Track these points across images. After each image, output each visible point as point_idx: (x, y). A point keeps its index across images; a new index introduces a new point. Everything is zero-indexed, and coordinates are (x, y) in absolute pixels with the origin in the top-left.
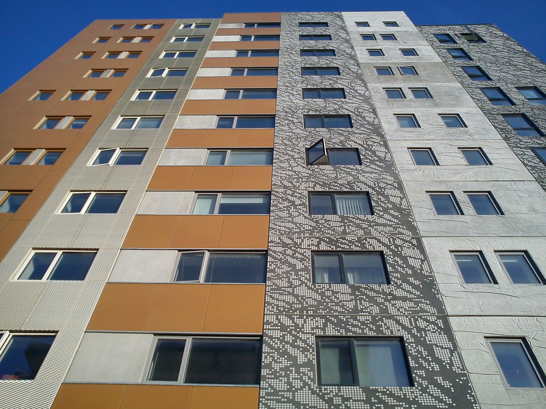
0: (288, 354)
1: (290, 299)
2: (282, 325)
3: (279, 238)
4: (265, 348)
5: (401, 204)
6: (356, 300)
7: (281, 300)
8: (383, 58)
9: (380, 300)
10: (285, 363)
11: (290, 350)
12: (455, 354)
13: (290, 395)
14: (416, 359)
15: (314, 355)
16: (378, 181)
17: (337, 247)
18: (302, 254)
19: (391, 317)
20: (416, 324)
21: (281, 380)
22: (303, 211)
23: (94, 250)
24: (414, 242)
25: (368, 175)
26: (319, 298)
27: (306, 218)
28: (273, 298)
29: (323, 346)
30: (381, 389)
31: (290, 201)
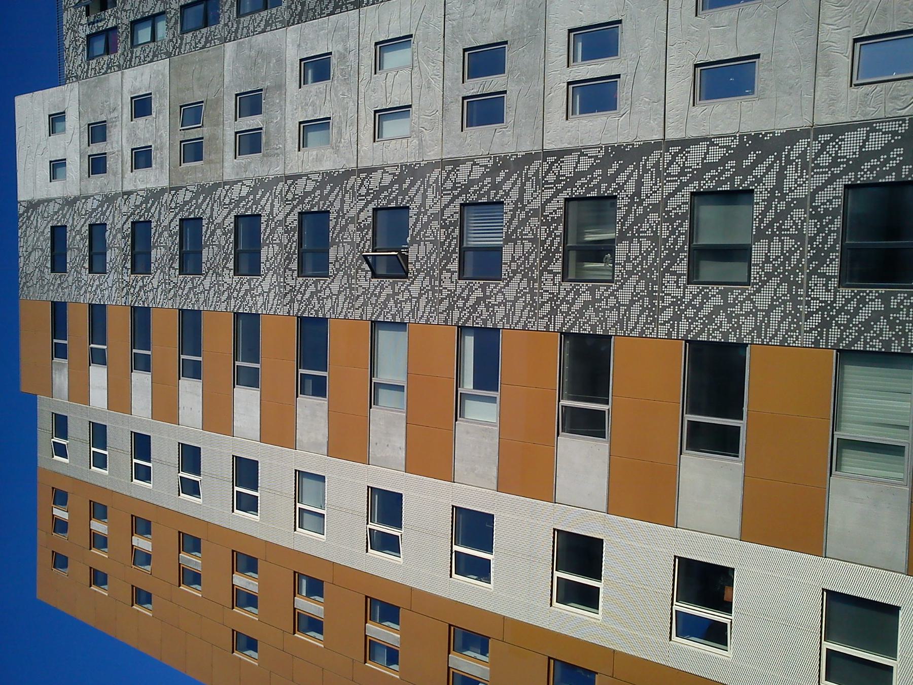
0: (711, 314)
1: (272, 295)
2: (672, 319)
3: (542, 318)
4: (575, 330)
5: (317, 181)
6: (522, 239)
7: (638, 319)
8: (157, 149)
9: (425, 219)
10: (315, 301)
11: (576, 307)
12: (387, 169)
13: (509, 305)
14: (589, 190)
15: (871, 292)
16: (285, 201)
17: (454, 251)
18: (301, 285)
19: (543, 206)
20: (551, 183)
21: (743, 323)
22: (495, 288)
23: (675, 561)
24: (363, 175)
25: (116, 219)
26: (519, 276)
27: (507, 285)
28: (422, 316)
29: (697, 277)
30: (756, 224)
31: (140, 290)
